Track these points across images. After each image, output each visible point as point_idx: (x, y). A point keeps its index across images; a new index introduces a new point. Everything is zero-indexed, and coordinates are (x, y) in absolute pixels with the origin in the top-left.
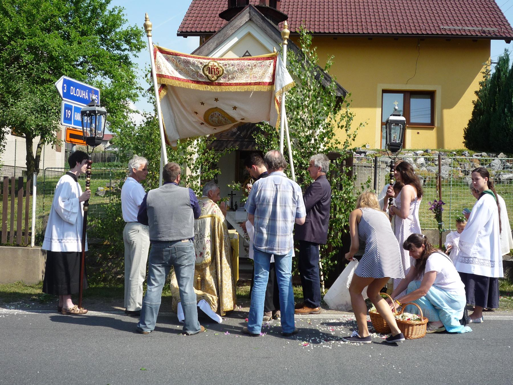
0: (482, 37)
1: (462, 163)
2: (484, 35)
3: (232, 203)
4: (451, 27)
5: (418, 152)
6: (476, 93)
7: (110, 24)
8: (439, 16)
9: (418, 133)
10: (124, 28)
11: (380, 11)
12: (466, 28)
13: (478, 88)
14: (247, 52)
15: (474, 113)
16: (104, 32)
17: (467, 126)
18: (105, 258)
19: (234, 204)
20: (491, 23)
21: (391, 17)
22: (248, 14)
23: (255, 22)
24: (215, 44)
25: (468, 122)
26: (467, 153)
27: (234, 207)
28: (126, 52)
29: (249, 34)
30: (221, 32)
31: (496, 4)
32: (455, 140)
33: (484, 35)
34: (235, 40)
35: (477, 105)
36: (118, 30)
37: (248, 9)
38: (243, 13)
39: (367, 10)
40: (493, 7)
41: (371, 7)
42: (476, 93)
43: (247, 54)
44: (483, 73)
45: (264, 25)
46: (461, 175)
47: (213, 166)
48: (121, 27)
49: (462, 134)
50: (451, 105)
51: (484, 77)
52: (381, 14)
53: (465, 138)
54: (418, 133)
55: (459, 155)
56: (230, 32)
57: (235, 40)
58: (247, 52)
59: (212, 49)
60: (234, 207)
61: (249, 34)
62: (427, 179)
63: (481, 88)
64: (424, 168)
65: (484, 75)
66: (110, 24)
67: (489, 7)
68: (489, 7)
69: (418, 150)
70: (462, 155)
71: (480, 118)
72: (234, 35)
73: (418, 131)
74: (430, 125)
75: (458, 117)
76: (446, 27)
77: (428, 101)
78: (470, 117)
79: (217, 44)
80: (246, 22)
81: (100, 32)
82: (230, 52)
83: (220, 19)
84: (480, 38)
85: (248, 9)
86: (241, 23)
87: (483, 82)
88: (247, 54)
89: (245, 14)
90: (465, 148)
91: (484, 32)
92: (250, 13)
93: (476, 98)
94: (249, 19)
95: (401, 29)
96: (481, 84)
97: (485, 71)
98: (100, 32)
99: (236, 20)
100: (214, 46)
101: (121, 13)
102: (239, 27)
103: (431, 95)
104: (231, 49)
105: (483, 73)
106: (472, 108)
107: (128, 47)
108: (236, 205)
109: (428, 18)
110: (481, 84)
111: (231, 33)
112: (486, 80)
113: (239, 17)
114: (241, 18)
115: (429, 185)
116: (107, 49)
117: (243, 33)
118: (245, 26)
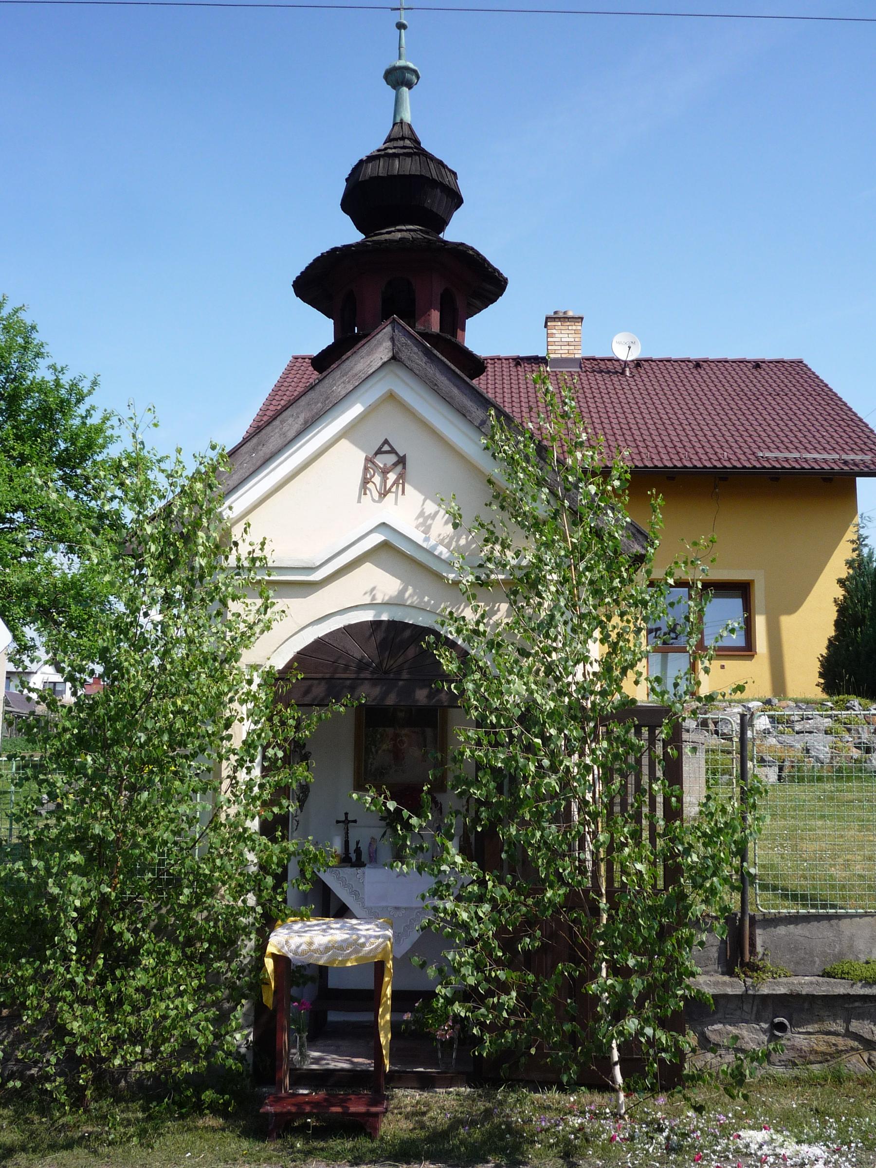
0: (842, 473)
1: (853, 727)
2: (846, 468)
3: (346, 844)
4: (777, 454)
5: (750, 705)
6: (841, 582)
7: (81, 442)
8: (750, 436)
9: (723, 667)
10: (113, 451)
11: (634, 427)
12: (808, 456)
13: (844, 572)
14: (386, 442)
15: (837, 624)
16: (69, 460)
17: (824, 652)
18: (53, 956)
19: (352, 847)
20: (854, 446)
21: (657, 439)
22: (388, 344)
23: (408, 363)
24: (301, 420)
25: (826, 643)
26: (856, 704)
27: (353, 856)
28: (115, 504)
29: (391, 397)
30: (318, 388)
31: (855, 415)
32: (805, 678)
33: (846, 468)
34: (356, 410)
35: (843, 609)
36: (99, 458)
37: (388, 329)
38: (374, 342)
39: (607, 426)
40: (852, 420)
41: (615, 421)
42: (841, 582)
43: (386, 448)
44: (853, 542)
45: (432, 371)
46: (856, 754)
47: (297, 752)
48: (105, 451)
49: (816, 667)
50: (793, 607)
51: (854, 550)
52: (637, 433)
53: (821, 675)
54: (723, 667)
55: (841, 709)
56: (340, 390)
57: (356, 410)
58: (386, 442)
59: (291, 434)
60: (353, 856)
61: (391, 397)
62: (787, 764)
63: (851, 571)
64: (772, 741)
65: (855, 546)
66: (81, 442)
67: (843, 420)
68: (843, 420)
69: (748, 701)
70: (848, 709)
71: (856, 632)
72: (353, 397)
73: (723, 662)
74: (747, 650)
75: (810, 627)
76: (768, 454)
77: (738, 603)
78: (831, 632)
79: (306, 422)
80: (384, 364)
81: (62, 461)
82: (344, 443)
83: (311, 368)
84: (838, 473)
85: (388, 329)
86: (369, 366)
87: (854, 560)
88: (386, 448)
89: (380, 344)
90: (825, 696)
91: (846, 463)
92: (392, 339)
93: (840, 593)
94: (390, 354)
95: (681, 460)
96: (850, 564)
97: (855, 537)
98: (62, 461)
99: (356, 358)
100: (297, 426)
101: (109, 423)
102: (364, 376)
103: (742, 590)
104: (346, 433)
105: (853, 542)
106: (832, 614)
107: (119, 493)
108: (358, 851)
109: (730, 439)
110: (850, 564)
111: (343, 393)
112: (859, 555)
113: (364, 351)
114: (369, 354)
115: (792, 779)
116: (77, 497)
117: (375, 391)
118: (382, 374)
